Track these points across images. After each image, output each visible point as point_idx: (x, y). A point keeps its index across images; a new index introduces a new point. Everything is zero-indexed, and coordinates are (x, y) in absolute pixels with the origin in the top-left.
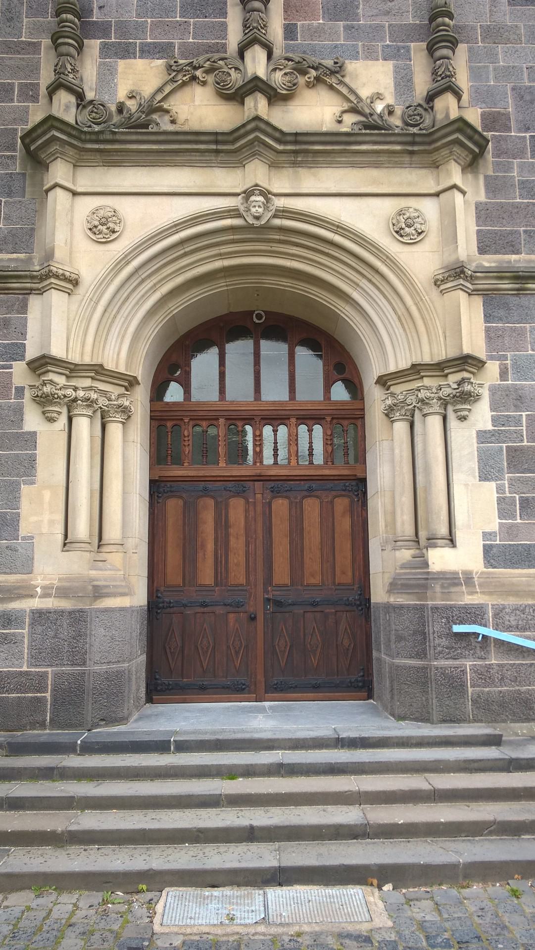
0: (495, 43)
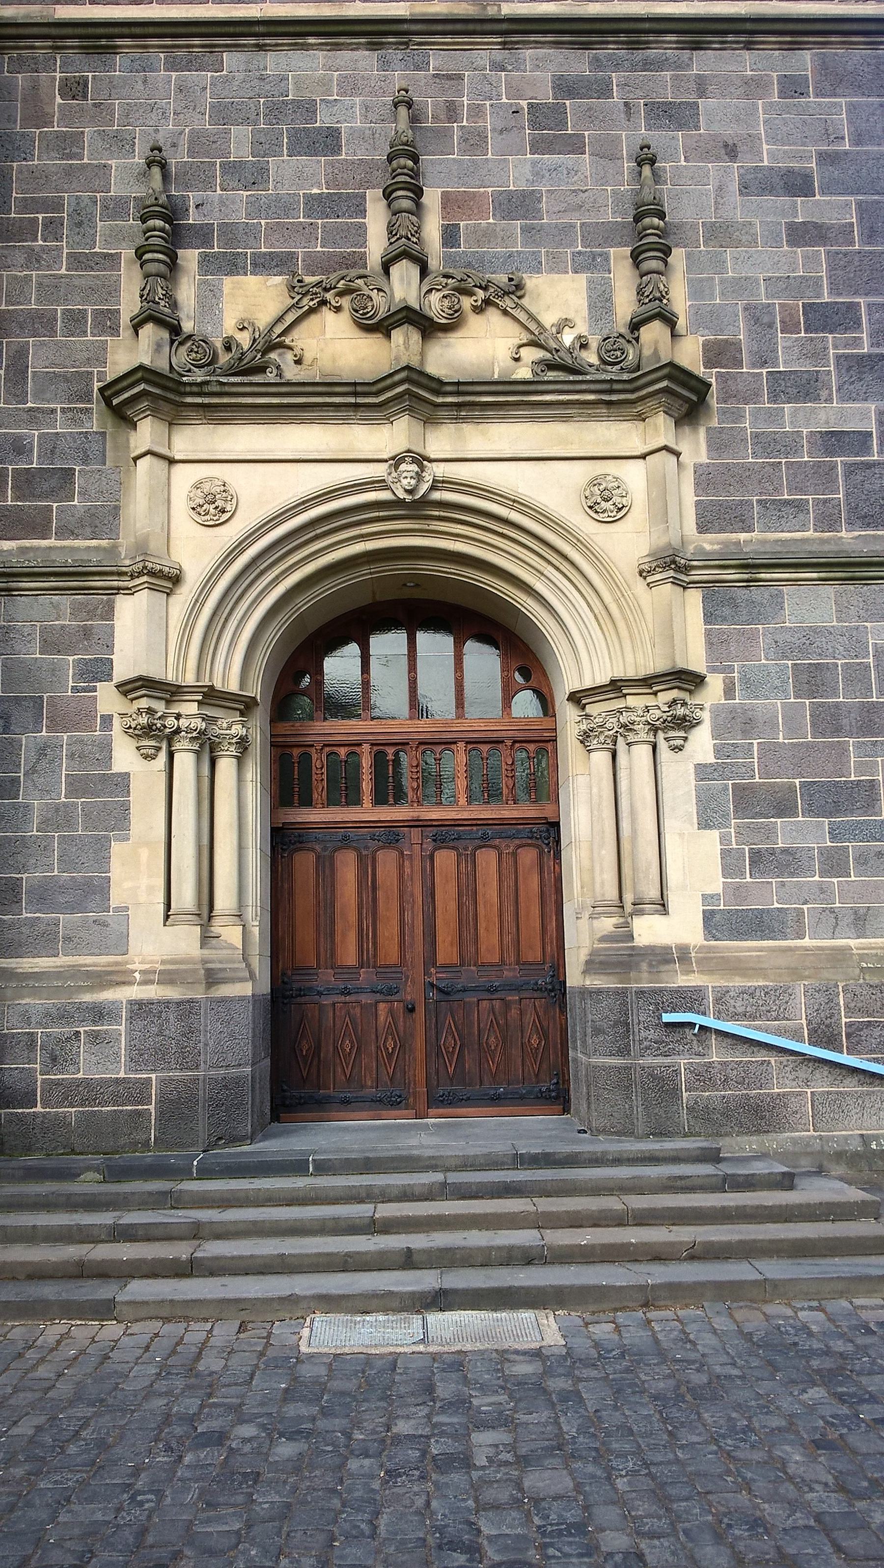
0: (721, 246)
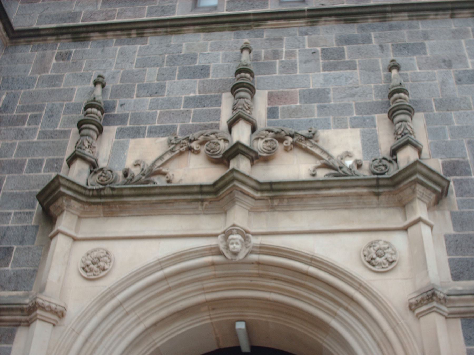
0: (448, 110)
